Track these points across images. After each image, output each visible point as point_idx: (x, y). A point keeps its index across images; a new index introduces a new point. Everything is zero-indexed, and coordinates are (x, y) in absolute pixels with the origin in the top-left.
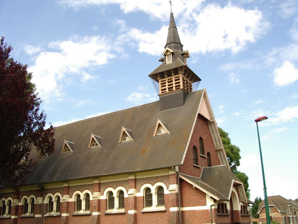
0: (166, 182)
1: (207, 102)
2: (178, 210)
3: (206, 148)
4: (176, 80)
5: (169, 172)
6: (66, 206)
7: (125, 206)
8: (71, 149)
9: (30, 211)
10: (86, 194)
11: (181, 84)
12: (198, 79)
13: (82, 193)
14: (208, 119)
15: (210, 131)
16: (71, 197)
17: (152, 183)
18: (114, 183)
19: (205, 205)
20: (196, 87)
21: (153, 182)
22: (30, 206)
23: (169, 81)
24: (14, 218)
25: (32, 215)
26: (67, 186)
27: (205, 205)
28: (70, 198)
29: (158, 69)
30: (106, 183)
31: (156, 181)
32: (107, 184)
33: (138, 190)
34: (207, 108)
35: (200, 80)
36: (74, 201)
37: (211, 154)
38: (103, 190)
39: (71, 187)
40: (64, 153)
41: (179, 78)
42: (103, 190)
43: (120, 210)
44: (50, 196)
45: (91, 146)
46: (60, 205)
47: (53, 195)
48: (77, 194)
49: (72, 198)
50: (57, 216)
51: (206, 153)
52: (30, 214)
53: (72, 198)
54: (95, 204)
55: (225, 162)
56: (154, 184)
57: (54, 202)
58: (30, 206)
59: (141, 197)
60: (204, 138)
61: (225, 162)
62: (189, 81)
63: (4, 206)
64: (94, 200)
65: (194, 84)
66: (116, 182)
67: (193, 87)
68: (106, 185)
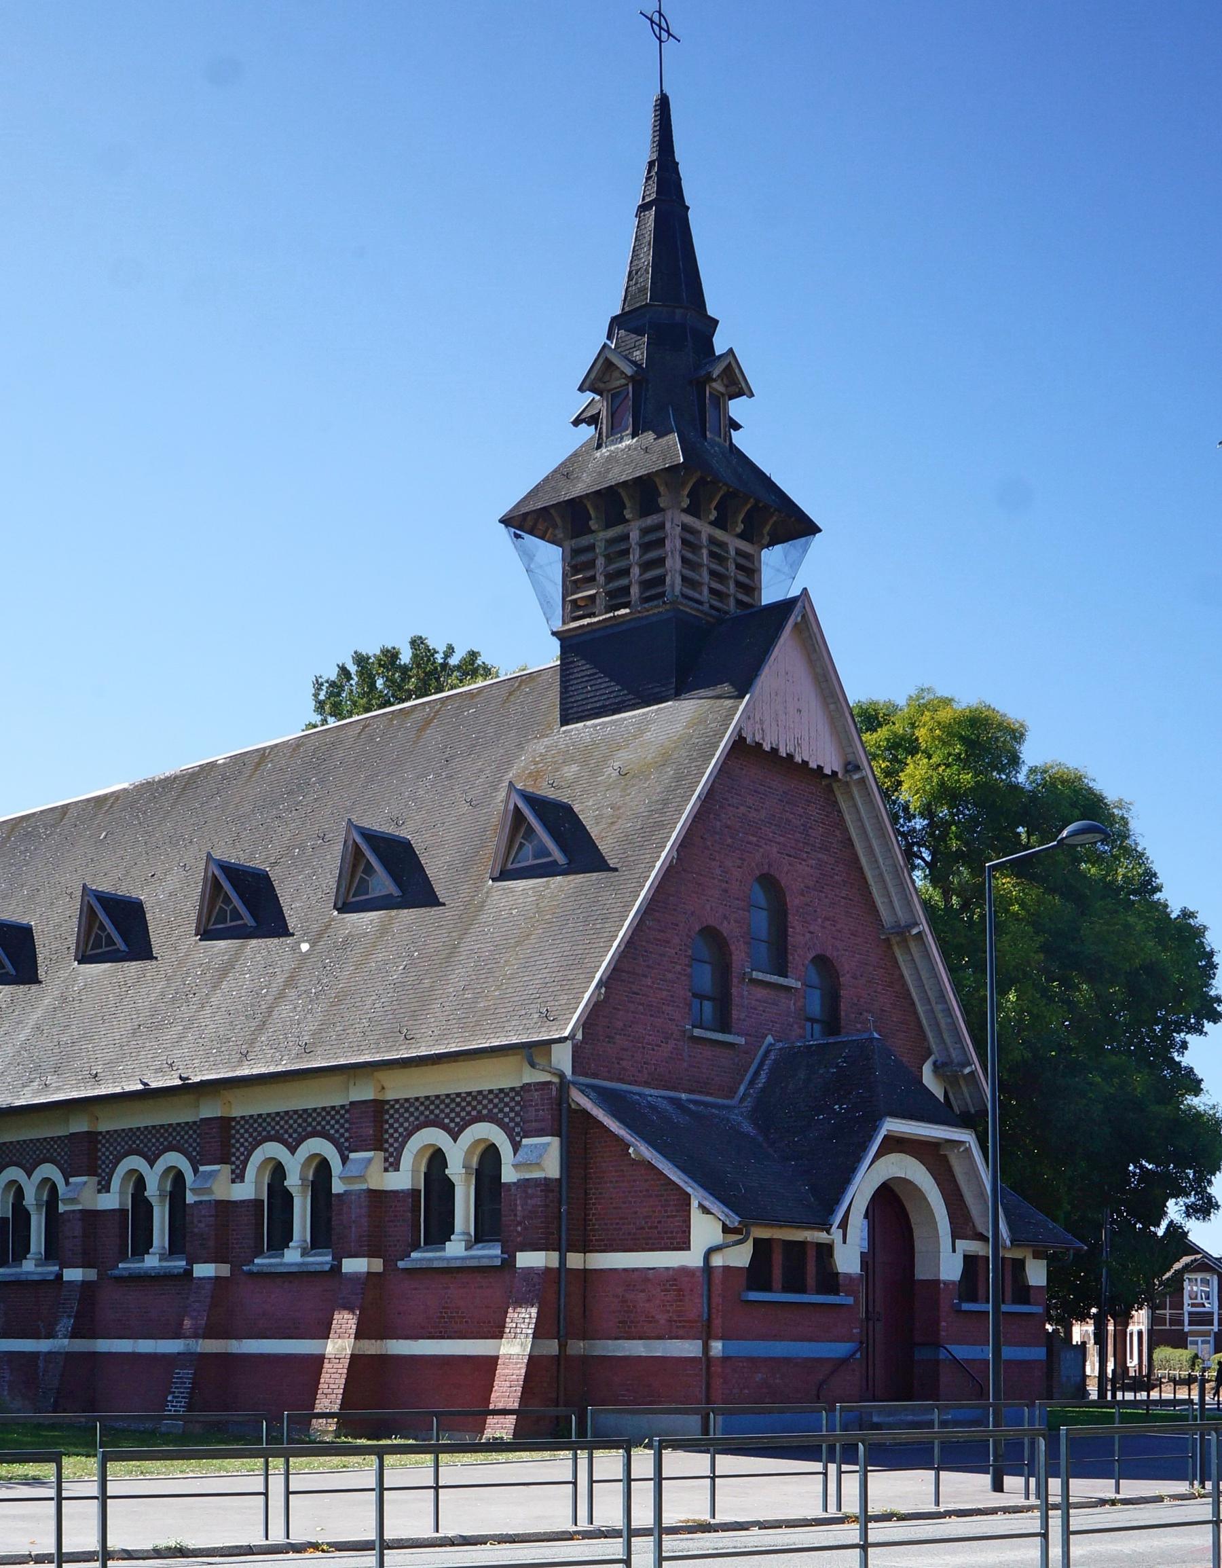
0: (512, 1124)
1: (819, 670)
2: (556, 1265)
3: (798, 935)
4: (609, 559)
5: (347, 1089)
6: (78, 1232)
7: (334, 1238)
8: (242, 910)
9: (167, 1246)
10: (431, 1151)
11: (674, 564)
12: (796, 526)
13: (293, 1154)
14: (828, 771)
15: (846, 830)
16: (105, 1188)
17: (452, 1125)
18: (291, 1122)
19: (685, 1245)
20: (779, 575)
21: (457, 1120)
22: (37, 1224)
23: (647, 539)
24: (365, 1269)
25: (323, 1260)
26: (86, 1129)
27: (685, 1245)
28: (386, 1170)
29: (565, 472)
30: (255, 1121)
31: (469, 1113)
32: (260, 1125)
33: (391, 1160)
34: (826, 704)
35: (809, 528)
36: (117, 1206)
37: (847, 965)
38: (242, 1154)
39: (238, 1123)
40: (88, 953)
41: (660, 534)
42: (242, 1154)
43: (483, 1248)
44: (15, 1181)
45: (209, 920)
46: (329, 1205)
47: (29, 1176)
48: (269, 1160)
49: (108, 1191)
50: (42, 1282)
51: (800, 957)
52: (166, 1260)
53: (108, 1191)
54: (202, 1225)
55: (943, 1011)
56: (462, 1129)
57: (154, 1201)
58: (37, 1224)
59: (402, 1191)
60: (796, 877)
61: (943, 1011)
62: (735, 544)
63: (21, 1214)
64: (201, 1202)
65: (772, 558)
66: (300, 1116)
67: (767, 575)
68: (255, 1130)
